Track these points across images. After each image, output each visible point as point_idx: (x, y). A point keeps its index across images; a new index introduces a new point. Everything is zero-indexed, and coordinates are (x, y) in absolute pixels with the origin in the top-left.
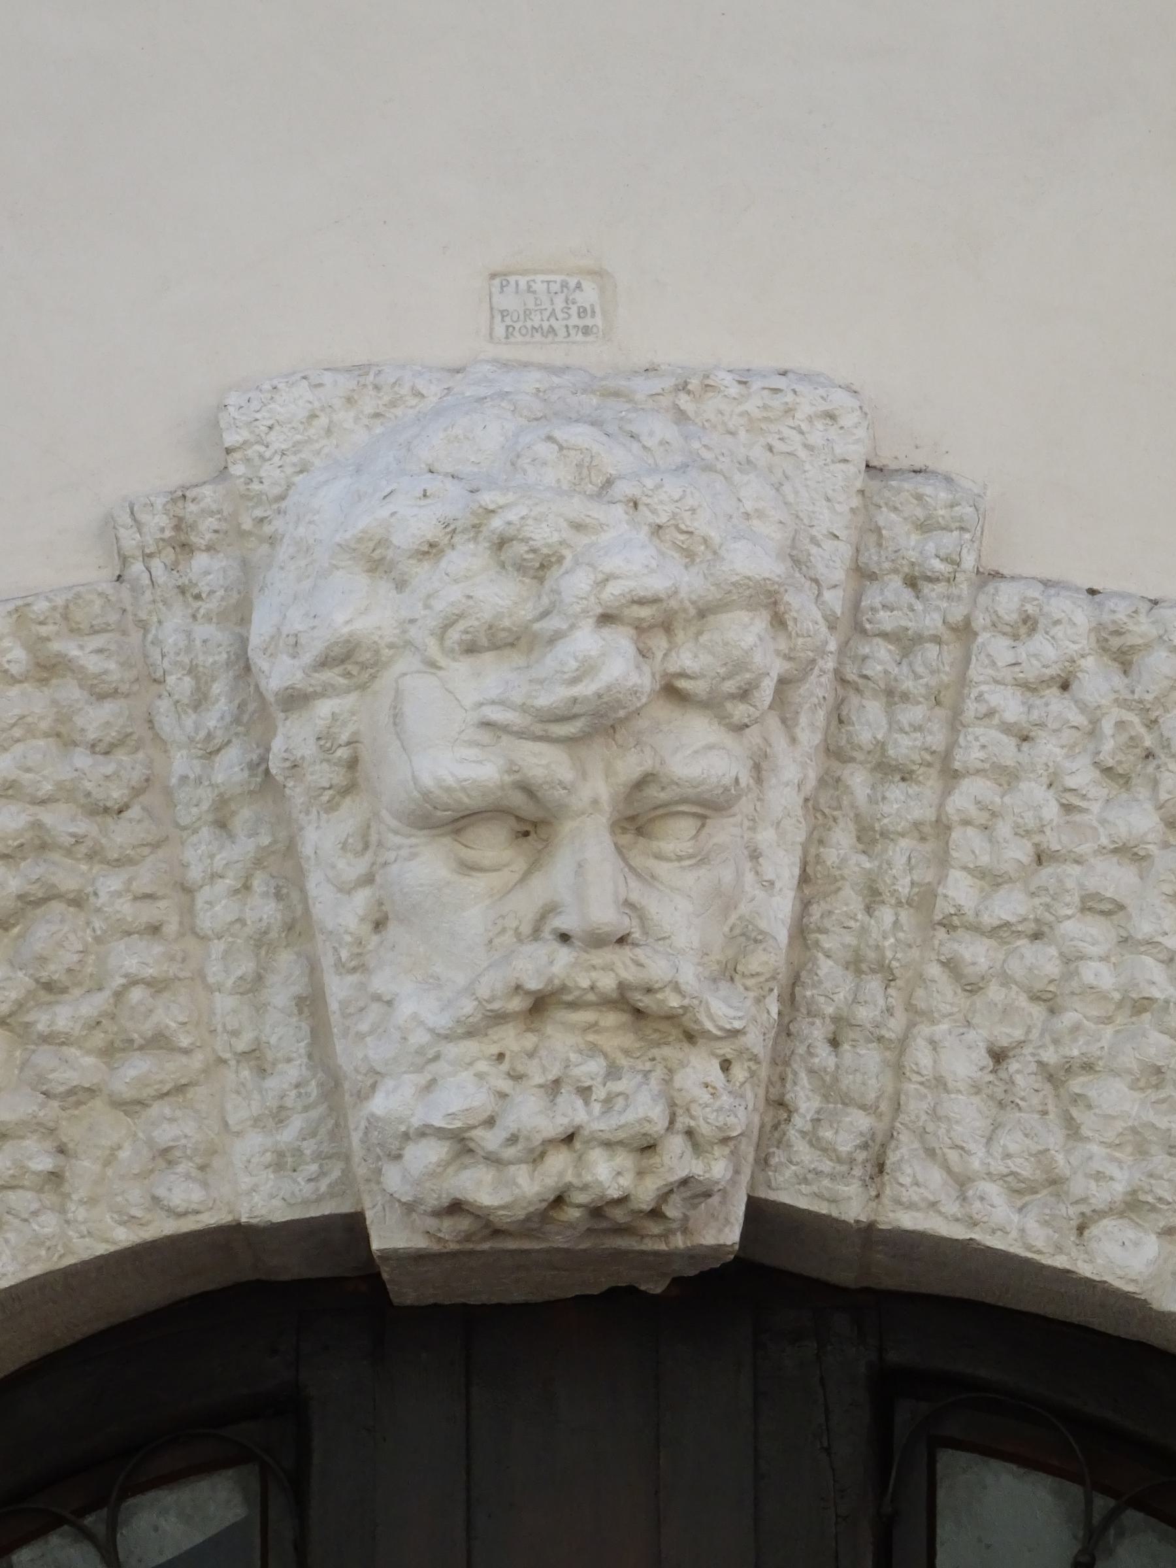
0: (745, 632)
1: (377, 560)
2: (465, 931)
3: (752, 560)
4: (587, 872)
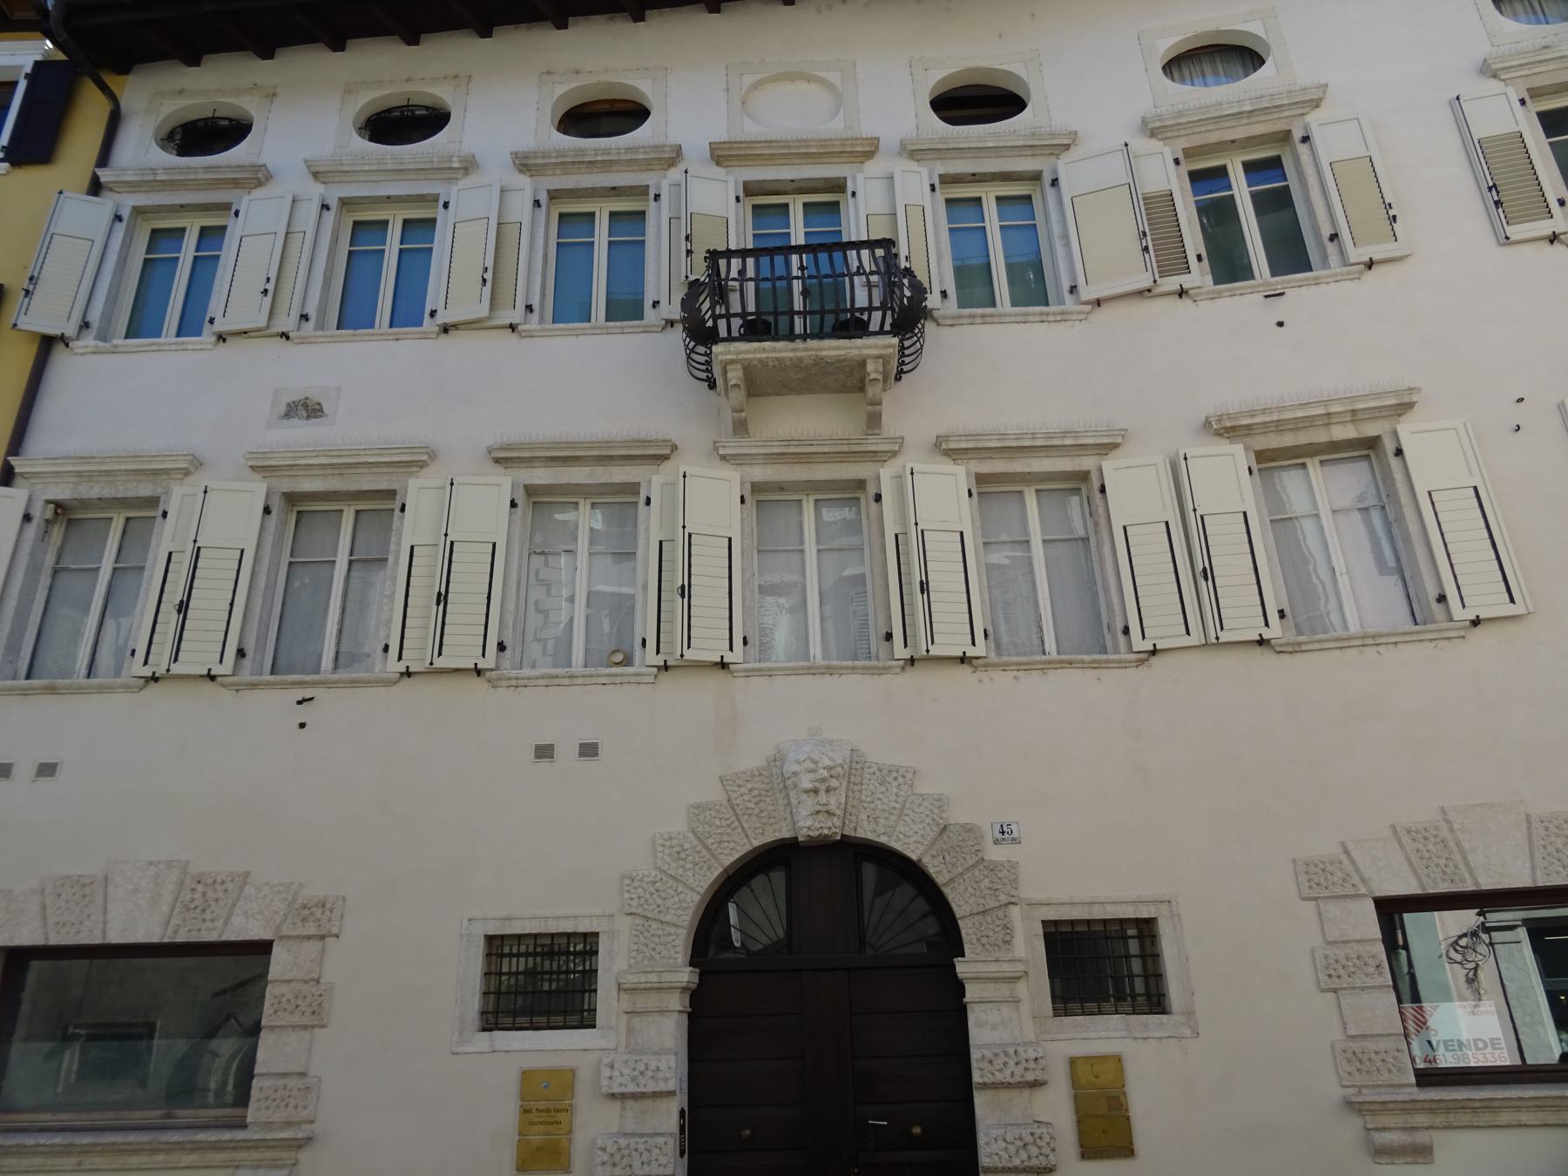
0: (839, 769)
1: (798, 762)
2: (808, 805)
3: (840, 761)
4: (822, 797)
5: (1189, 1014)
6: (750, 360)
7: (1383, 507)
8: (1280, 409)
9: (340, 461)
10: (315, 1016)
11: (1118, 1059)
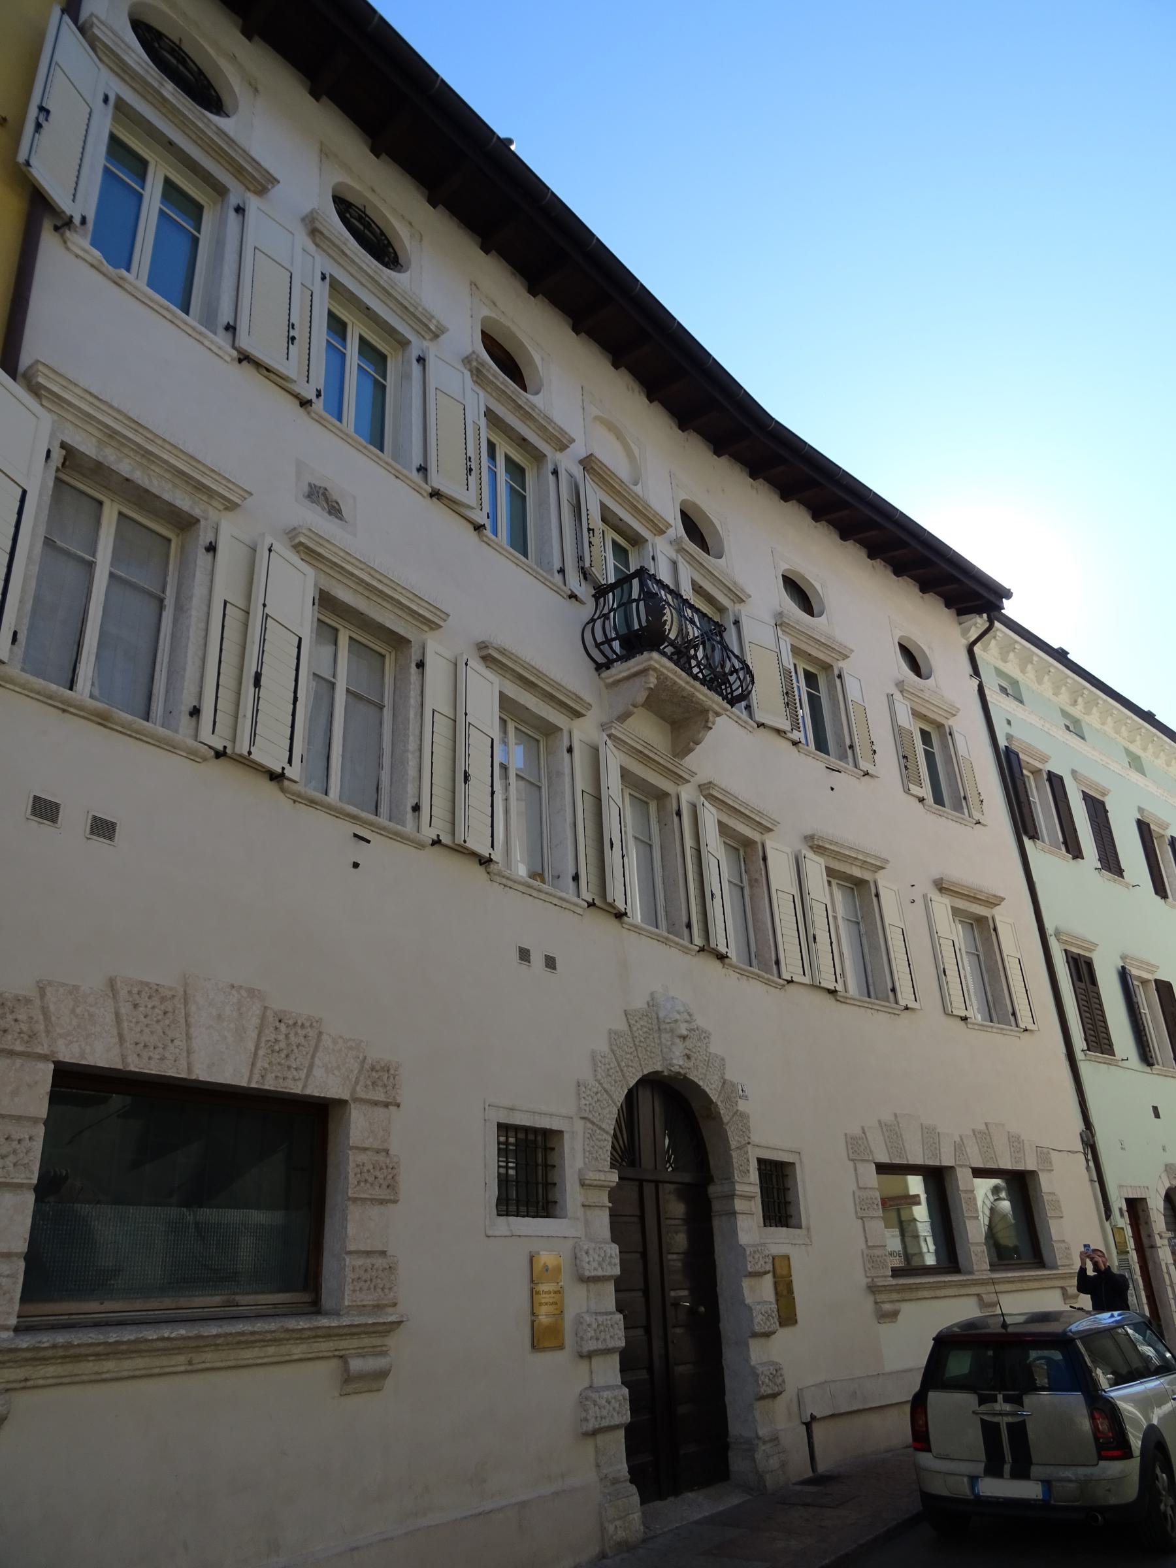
1: (679, 1013)
5: (808, 1229)
6: (666, 678)
7: (858, 923)
8: (843, 846)
9: (380, 586)
10: (388, 1189)
11: (787, 1258)
